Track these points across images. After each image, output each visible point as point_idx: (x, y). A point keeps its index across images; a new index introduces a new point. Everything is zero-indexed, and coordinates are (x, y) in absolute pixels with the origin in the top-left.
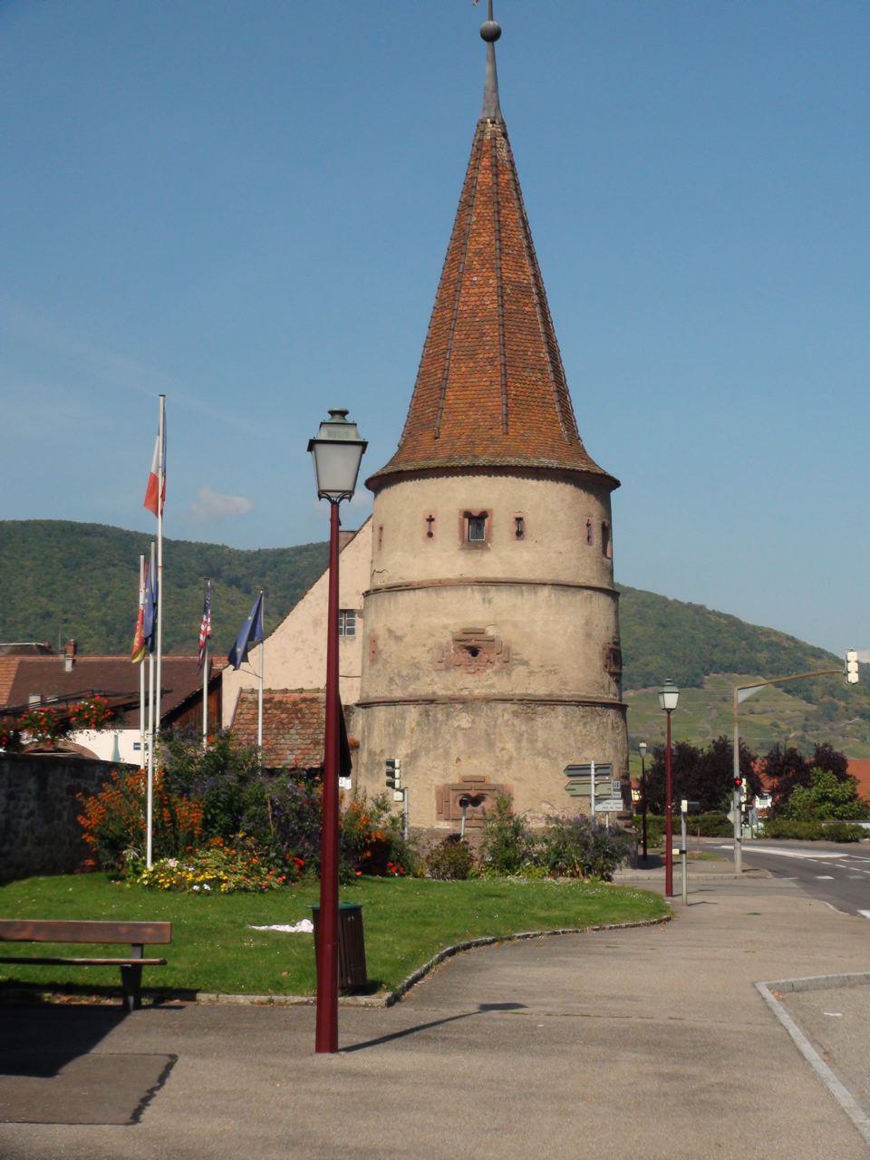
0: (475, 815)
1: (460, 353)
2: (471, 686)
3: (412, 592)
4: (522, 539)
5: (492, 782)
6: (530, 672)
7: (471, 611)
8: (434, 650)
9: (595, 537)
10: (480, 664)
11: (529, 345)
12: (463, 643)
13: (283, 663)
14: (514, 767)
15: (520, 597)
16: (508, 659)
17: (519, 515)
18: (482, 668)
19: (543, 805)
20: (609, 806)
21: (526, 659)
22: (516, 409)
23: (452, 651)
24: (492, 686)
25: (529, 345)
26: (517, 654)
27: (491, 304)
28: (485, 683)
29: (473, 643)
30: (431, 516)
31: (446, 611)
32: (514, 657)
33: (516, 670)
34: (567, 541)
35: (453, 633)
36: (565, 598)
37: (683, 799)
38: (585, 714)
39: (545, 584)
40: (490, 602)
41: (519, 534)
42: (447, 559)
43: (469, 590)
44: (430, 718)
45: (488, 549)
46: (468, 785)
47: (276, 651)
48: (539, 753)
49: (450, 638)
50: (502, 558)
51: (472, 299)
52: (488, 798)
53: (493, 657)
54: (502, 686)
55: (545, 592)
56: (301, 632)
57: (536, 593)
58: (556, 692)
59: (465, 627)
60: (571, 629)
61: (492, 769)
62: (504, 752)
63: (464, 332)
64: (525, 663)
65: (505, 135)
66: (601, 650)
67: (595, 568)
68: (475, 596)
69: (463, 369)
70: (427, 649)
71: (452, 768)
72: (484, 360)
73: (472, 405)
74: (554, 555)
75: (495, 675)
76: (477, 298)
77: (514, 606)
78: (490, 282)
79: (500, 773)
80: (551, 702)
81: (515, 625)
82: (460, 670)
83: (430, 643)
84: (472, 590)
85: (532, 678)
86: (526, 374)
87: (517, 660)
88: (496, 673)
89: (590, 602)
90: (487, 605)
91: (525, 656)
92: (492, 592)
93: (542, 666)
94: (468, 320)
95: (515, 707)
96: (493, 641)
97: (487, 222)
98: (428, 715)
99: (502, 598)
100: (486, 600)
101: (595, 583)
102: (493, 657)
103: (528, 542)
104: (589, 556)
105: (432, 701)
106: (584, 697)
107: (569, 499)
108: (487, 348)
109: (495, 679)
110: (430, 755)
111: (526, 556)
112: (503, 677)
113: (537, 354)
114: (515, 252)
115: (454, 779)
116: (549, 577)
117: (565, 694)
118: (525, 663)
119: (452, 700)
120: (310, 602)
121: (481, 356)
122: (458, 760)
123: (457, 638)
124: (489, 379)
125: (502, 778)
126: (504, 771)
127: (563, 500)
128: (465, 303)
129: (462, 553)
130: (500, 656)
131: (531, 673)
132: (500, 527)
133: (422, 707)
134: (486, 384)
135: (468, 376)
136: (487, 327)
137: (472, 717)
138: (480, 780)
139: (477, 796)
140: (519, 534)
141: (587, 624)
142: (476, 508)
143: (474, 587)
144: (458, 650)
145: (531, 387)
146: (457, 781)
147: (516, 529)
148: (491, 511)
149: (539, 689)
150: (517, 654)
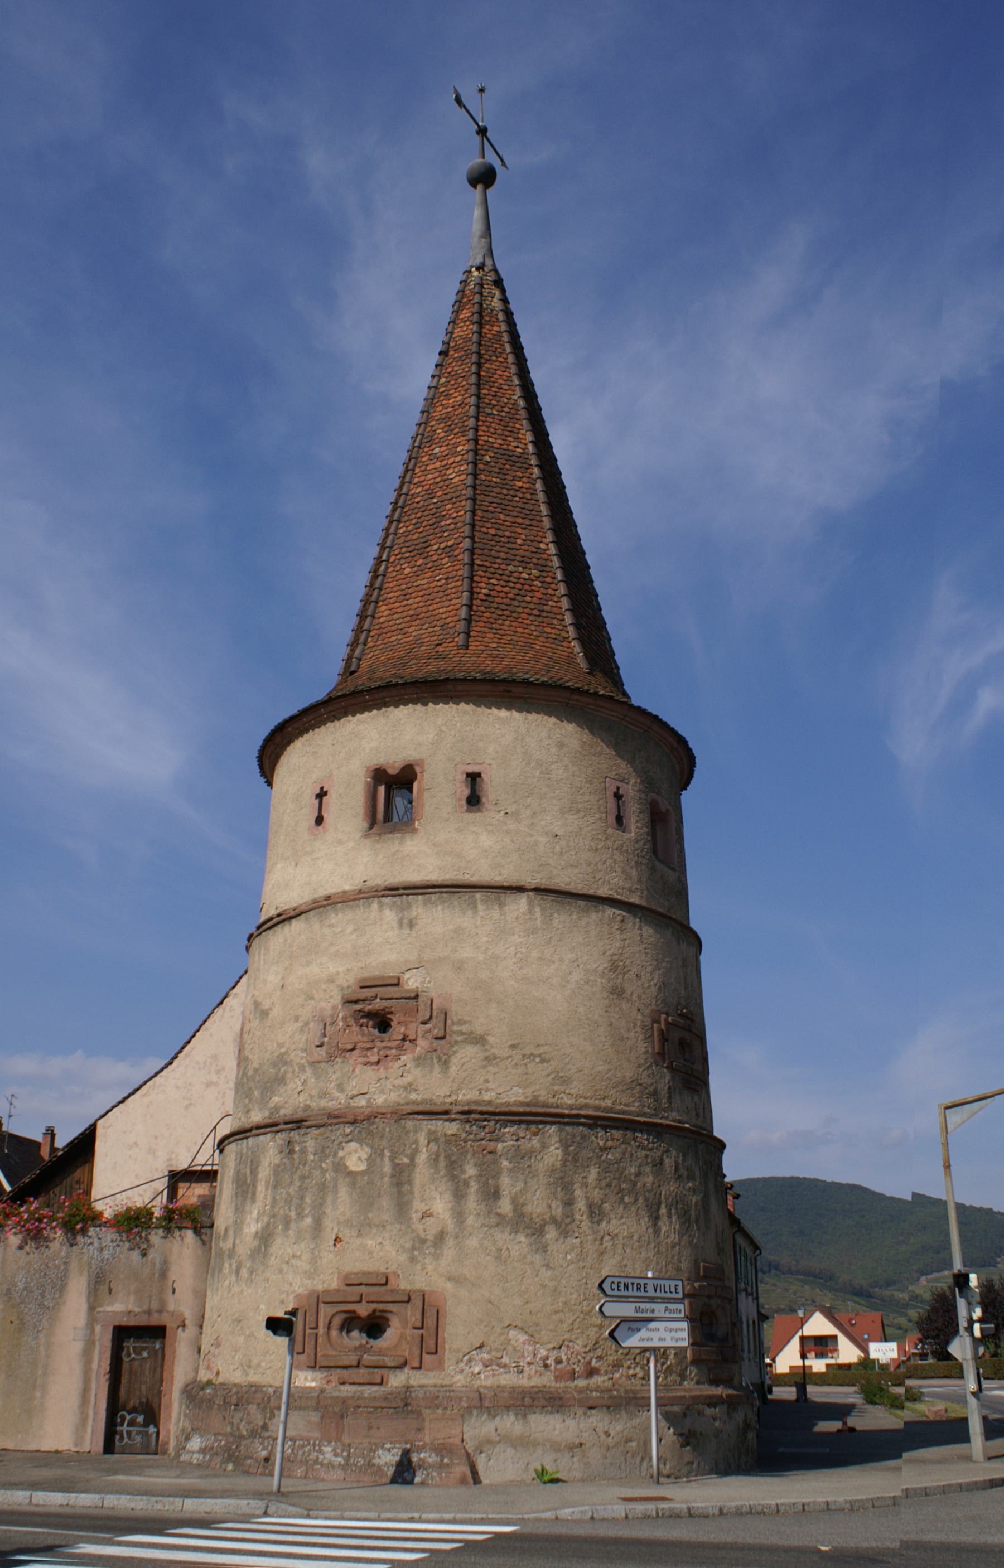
1: (404, 550)
3: (286, 925)
4: (479, 811)
5: (404, 1285)
6: (486, 1058)
7: (381, 944)
8: (312, 1025)
9: (633, 820)
10: (390, 1044)
11: (519, 530)
12: (358, 1007)
13: (187, 1107)
14: (449, 1251)
15: (470, 913)
16: (442, 1029)
19: (512, 1333)
20: (655, 1335)
22: (488, 615)
23: (341, 1024)
24: (409, 1087)
25: (519, 530)
26: (461, 1022)
27: (458, 476)
28: (397, 1082)
29: (378, 1005)
30: (322, 788)
31: (333, 950)
32: (455, 1028)
33: (459, 1055)
34: (571, 818)
35: (342, 989)
36: (563, 918)
37: (901, 1349)
38: (610, 1144)
39: (520, 889)
40: (411, 925)
41: (474, 801)
42: (345, 856)
43: (375, 906)
44: (295, 1156)
45: (414, 831)
47: (177, 1087)
48: (501, 1221)
49: (337, 999)
50: (439, 844)
51: (430, 476)
52: (395, 1322)
53: (413, 1029)
54: (434, 1086)
55: (520, 904)
56: (215, 1057)
57: (501, 905)
58: (544, 1096)
60: (576, 976)
61: (403, 1258)
62: (430, 1221)
63: (414, 522)
64: (480, 1040)
65: (498, 283)
66: (648, 1021)
67: (634, 873)
68: (385, 916)
69: (407, 571)
70: (300, 1024)
71: (328, 1257)
72: (439, 552)
73: (414, 617)
74: (542, 839)
75: (418, 1066)
76: (437, 474)
77: (458, 931)
78: (459, 449)
79: (419, 1267)
80: (530, 1117)
81: (459, 967)
83: (305, 1013)
84: (381, 906)
85: (491, 1069)
86: (511, 568)
87: (462, 1033)
88: (419, 1061)
89: (621, 930)
90: (406, 931)
93: (513, 1047)
94: (422, 503)
96: (416, 997)
97: (460, 380)
98: (291, 1152)
99: (436, 919)
100: (405, 921)
101: (635, 899)
102: (413, 1029)
103: (490, 815)
105: (297, 1123)
106: (610, 1110)
107: (574, 744)
108: (446, 534)
109: (417, 1072)
110: (291, 1232)
111: (486, 841)
113: (535, 544)
115: (329, 1281)
117: (567, 1101)
118: (480, 1040)
119: (334, 1118)
120: (232, 1009)
121: (435, 547)
122: (337, 1240)
124: (445, 576)
125: (426, 1276)
127: (561, 745)
128: (419, 484)
129: (368, 842)
130: (428, 1026)
132: (438, 792)
134: (439, 584)
135: (415, 578)
136: (449, 507)
139: (373, 1315)
140: (474, 801)
141: (614, 967)
142: (394, 761)
143: (387, 900)
144: (352, 1022)
145: (519, 586)
147: (467, 792)
148: (421, 763)
149: (505, 1090)
150: (461, 1022)
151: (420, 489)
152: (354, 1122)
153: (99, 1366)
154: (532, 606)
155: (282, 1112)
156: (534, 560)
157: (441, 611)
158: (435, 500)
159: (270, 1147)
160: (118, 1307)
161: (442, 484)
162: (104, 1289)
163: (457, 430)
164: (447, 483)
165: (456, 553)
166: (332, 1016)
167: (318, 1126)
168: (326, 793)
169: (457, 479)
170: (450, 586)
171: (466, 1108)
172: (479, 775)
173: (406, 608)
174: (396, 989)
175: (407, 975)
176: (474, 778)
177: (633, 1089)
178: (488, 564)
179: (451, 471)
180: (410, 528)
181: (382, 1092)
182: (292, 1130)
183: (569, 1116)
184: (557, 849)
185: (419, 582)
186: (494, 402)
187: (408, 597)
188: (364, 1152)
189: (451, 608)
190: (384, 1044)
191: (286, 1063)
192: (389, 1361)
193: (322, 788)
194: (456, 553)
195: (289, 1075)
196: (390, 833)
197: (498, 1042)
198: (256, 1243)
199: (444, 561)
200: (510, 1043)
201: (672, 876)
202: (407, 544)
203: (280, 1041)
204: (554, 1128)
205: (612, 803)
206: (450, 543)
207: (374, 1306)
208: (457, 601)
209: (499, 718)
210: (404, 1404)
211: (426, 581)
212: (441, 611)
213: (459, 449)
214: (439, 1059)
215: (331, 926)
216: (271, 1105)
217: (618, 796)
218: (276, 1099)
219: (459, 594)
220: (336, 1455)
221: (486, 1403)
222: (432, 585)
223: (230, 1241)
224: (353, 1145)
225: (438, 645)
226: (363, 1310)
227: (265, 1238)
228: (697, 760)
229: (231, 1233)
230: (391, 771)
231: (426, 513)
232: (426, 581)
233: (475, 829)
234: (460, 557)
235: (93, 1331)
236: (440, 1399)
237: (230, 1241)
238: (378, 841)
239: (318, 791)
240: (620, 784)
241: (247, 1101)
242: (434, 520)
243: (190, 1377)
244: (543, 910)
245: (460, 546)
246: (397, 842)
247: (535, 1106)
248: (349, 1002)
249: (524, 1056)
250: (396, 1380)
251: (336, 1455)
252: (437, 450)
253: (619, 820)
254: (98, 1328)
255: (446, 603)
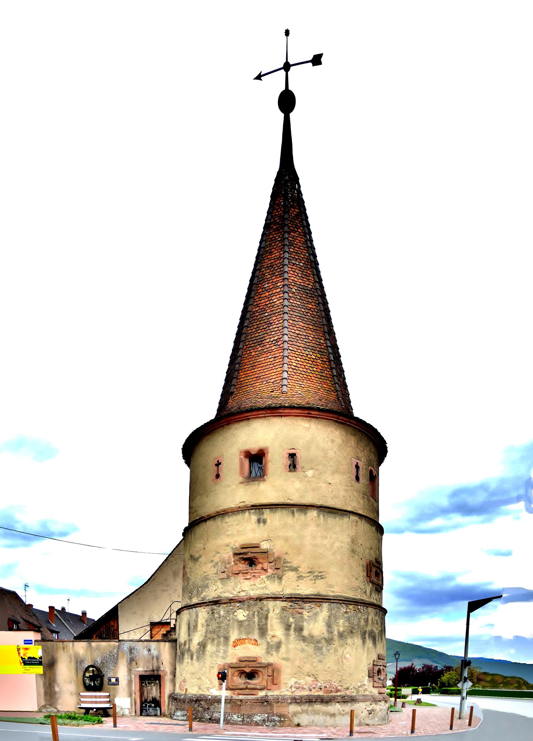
0: (249, 686)
2: (246, 589)
5: (263, 661)
6: (298, 577)
12: (241, 556)
14: (283, 649)
16: (279, 566)
17: (292, 452)
18: (256, 575)
21: (295, 566)
23: (233, 563)
29: (250, 555)
40: (265, 522)
45: (264, 480)
46: (243, 664)
49: (231, 554)
54: (273, 588)
55: (313, 513)
59: (244, 543)
64: (295, 569)
72: (270, 343)
74: (324, 485)
75: (268, 580)
81: (286, 539)
82: (241, 577)
84: (250, 513)
85: (300, 581)
87: (287, 567)
89: (356, 526)
90: (262, 524)
91: (295, 564)
92: (267, 514)
93: (309, 572)
95: (284, 604)
99: (274, 519)
100: (261, 520)
101: (361, 512)
103: (299, 473)
104: (357, 491)
105: (216, 602)
107: (339, 441)
108: (273, 333)
109: (268, 583)
111: (298, 485)
112: (274, 580)
114: (301, 264)
116: (319, 503)
118: (295, 569)
119: (231, 601)
121: (268, 340)
123: (236, 552)
126: (274, 653)
127: (333, 441)
131: (300, 577)
132: (276, 462)
133: (208, 608)
137: (247, 612)
138: (253, 659)
141: (353, 541)
142: (254, 446)
146: (235, 661)
148: (267, 449)
149: (306, 589)
151: (258, 308)
152: (240, 602)
153: (135, 688)
154: (317, 373)
155: (207, 598)
156: (318, 349)
157: (272, 374)
158: (266, 314)
159: (203, 613)
160: (141, 669)
161: (270, 305)
162: (134, 663)
163: (277, 274)
164: (273, 304)
165: (279, 343)
166: (228, 560)
167: (225, 603)
168: (220, 464)
169: (278, 302)
170: (277, 361)
171: (290, 596)
172: (295, 454)
173: (254, 373)
174: (258, 549)
175: (263, 543)
176: (292, 456)
177: (357, 590)
178: (296, 350)
179: (274, 297)
180: (254, 330)
181: (253, 590)
182: (213, 605)
183: (333, 600)
184: (330, 490)
185: (260, 360)
186: (297, 257)
187: (254, 367)
188: (246, 613)
189: (277, 373)
190: (253, 571)
191: (208, 579)
192: (258, 687)
193: (218, 461)
194: (279, 343)
195: (210, 584)
196: (253, 481)
197: (303, 569)
198: (198, 646)
199: (273, 348)
200: (308, 571)
201: (376, 505)
202: (253, 339)
203: (205, 571)
204: (327, 604)
205: (354, 470)
206: (275, 338)
207: (252, 668)
208: (280, 369)
209: (304, 427)
210: (265, 702)
211: (263, 359)
212: (272, 374)
213: (278, 285)
214: (278, 577)
215: (226, 523)
216: (202, 596)
217: (357, 467)
218: (204, 593)
219: (281, 366)
220: (238, 718)
221: (296, 701)
222: (267, 361)
223: (187, 646)
224: (241, 610)
225: (271, 392)
226: (248, 670)
227: (203, 646)
228: (388, 454)
229: (187, 643)
230: (253, 453)
231: (261, 322)
232: (263, 359)
233: (293, 480)
234: (281, 346)
235: (131, 677)
236: (278, 700)
237: (187, 646)
238: (247, 485)
239: (216, 463)
240: (358, 461)
241: (190, 594)
242: (266, 326)
243: (172, 692)
244: (324, 516)
245: (281, 339)
246: (256, 485)
247: (319, 596)
248: (235, 554)
249: (314, 576)
250: (262, 694)
251: (238, 718)
252: (266, 286)
253: (357, 478)
254: (133, 676)
255: (275, 370)
